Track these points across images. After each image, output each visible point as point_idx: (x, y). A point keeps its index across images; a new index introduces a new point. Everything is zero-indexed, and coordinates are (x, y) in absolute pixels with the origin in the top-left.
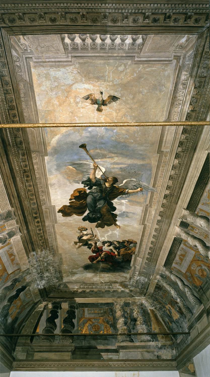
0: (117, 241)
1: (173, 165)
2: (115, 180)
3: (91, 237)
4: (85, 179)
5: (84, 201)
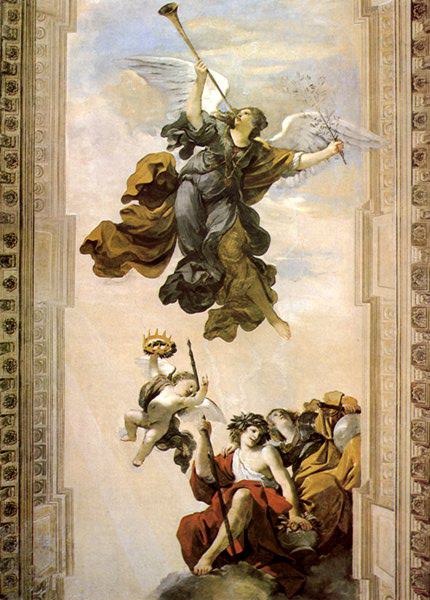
0: (285, 413)
1: (413, 42)
2: (260, 122)
3: (188, 394)
4: (172, 119)
5: (167, 209)
